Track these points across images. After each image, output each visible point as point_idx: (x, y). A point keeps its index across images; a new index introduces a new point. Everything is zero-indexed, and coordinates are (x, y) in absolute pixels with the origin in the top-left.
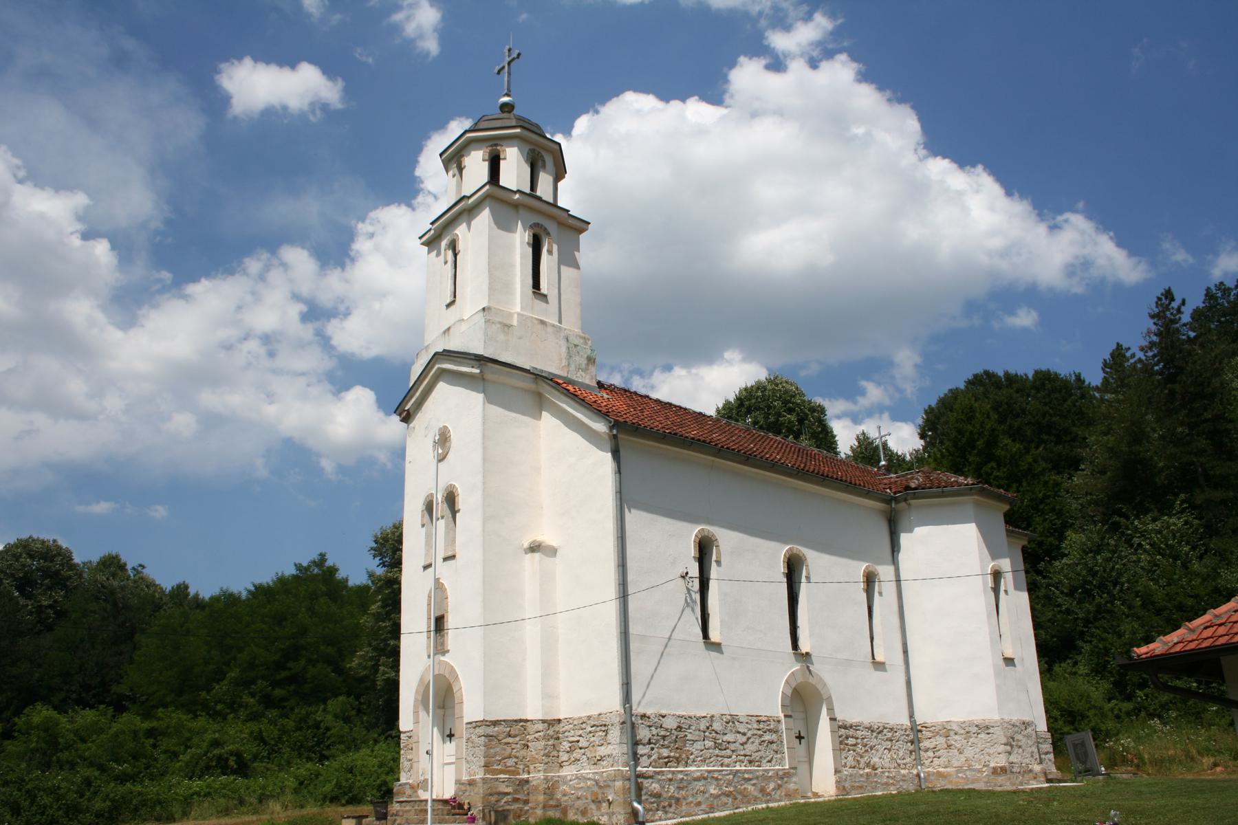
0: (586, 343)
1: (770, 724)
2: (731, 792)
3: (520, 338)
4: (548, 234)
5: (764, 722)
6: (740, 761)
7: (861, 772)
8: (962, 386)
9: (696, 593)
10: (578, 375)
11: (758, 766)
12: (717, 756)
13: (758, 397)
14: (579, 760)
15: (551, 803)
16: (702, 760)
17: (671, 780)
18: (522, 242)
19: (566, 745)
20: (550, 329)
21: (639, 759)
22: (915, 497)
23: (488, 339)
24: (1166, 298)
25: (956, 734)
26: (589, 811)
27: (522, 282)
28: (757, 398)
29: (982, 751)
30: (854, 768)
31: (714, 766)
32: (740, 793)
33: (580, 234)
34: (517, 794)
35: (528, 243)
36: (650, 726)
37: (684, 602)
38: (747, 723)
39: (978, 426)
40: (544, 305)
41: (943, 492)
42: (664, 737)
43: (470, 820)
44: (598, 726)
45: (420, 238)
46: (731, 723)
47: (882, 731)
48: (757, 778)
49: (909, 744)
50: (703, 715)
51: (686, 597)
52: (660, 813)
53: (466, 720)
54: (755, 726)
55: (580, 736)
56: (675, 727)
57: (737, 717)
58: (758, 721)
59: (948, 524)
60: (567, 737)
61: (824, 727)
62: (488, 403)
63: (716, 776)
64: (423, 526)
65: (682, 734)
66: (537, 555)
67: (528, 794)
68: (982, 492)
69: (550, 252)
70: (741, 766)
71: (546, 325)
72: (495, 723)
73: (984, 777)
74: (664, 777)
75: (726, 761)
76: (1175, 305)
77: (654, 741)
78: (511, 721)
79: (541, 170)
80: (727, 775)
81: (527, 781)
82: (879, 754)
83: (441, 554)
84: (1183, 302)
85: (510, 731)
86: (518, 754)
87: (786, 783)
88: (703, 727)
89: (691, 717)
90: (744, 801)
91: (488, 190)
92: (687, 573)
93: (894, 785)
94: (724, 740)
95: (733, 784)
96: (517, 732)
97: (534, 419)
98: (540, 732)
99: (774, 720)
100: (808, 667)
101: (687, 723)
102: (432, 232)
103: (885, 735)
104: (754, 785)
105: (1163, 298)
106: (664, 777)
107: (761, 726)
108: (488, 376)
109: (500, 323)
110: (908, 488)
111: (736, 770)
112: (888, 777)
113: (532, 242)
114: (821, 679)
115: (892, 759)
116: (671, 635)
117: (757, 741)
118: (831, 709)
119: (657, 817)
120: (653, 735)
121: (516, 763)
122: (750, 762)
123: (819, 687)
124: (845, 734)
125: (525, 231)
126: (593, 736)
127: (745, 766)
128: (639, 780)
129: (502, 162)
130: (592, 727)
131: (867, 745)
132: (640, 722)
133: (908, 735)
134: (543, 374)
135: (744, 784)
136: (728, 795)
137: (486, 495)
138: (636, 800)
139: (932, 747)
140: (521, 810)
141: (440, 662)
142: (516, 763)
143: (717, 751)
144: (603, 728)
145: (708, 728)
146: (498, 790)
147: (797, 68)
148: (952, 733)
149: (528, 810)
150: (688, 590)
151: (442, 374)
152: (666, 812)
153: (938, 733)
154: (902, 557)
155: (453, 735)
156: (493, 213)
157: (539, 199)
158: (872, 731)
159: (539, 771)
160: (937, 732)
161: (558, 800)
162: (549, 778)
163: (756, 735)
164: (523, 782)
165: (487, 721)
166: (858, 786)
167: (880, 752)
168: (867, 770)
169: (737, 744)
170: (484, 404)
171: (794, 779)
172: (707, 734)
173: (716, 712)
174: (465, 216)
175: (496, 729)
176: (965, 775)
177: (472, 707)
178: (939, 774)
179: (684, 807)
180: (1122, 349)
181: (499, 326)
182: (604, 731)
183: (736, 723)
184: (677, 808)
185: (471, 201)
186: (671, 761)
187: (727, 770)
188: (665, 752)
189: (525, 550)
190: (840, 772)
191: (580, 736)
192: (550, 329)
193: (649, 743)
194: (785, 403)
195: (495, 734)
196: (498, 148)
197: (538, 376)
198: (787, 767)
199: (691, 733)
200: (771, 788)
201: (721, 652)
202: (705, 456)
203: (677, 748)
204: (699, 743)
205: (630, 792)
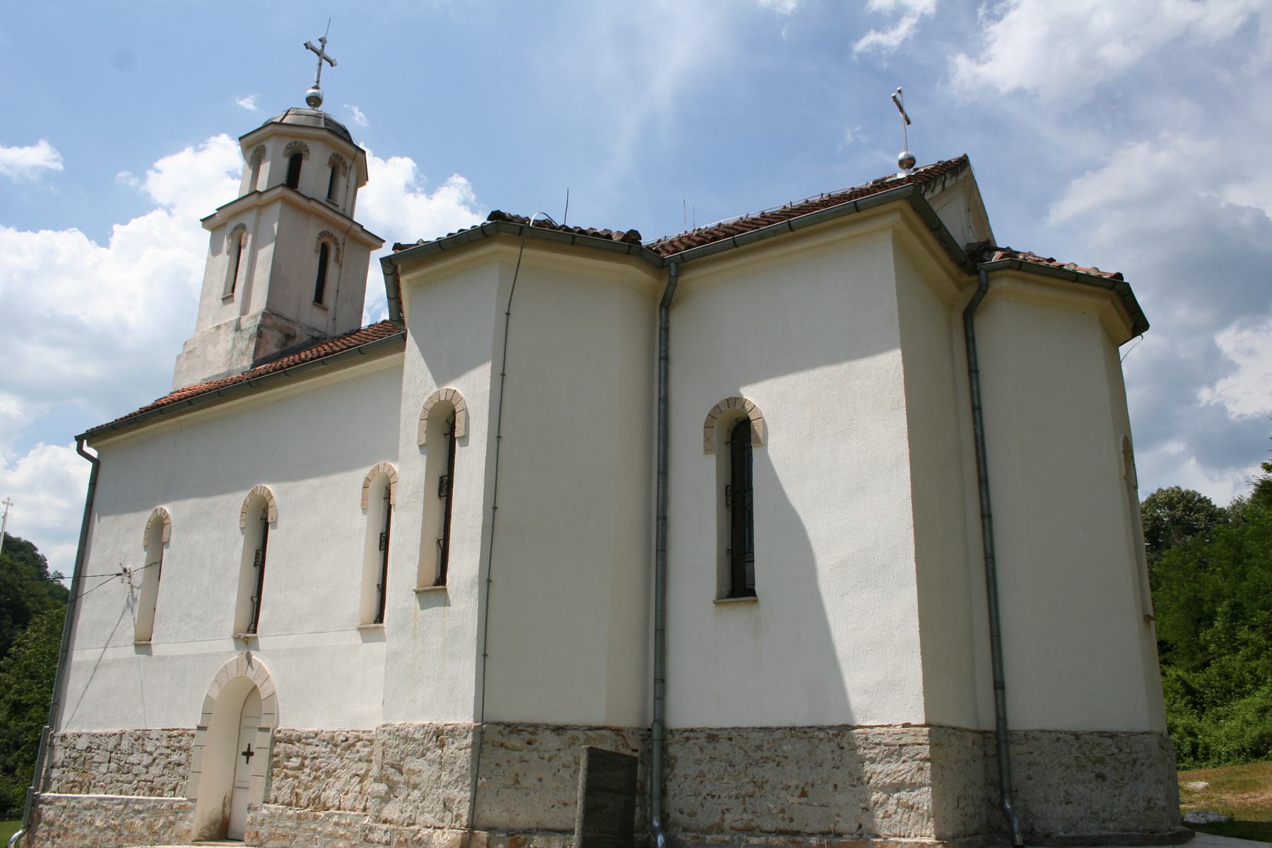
1: (181, 740)
5: (175, 737)
8: (1125, 281)
11: (158, 796)
31: (112, 794)
37: (125, 602)
38: (157, 739)
42: (75, 759)
51: (129, 596)
58: (169, 737)
63: (104, 805)
75: (126, 786)
88: (110, 747)
103: (358, 752)
104: (143, 819)
112: (337, 824)
131: (320, 768)
135: (133, 817)
145: (116, 747)
155: (252, 754)
158: (336, 745)
171: (190, 816)
172: (113, 754)
187: (118, 799)
199: (98, 754)
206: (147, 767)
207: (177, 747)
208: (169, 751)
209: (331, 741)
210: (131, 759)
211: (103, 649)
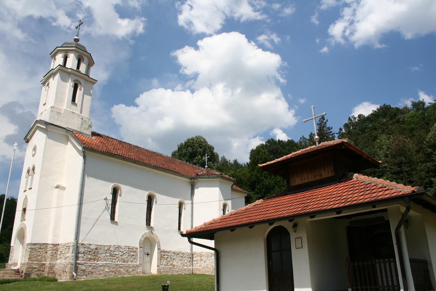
0: (89, 120)
1: (133, 249)
2: (114, 271)
3: (64, 117)
4: (81, 84)
5: (131, 248)
6: (119, 261)
7: (168, 267)
9: (110, 205)
10: (85, 131)
11: (126, 263)
12: (110, 259)
13: (191, 142)
14: (62, 258)
15: (51, 271)
16: (104, 260)
17: (90, 266)
18: (70, 85)
19: (59, 253)
20: (76, 115)
21: (79, 258)
23: (51, 117)
24: (322, 119)
25: (204, 256)
27: (68, 99)
28: (190, 143)
29: (212, 262)
30: (166, 265)
31: (109, 262)
32: (118, 271)
33: (94, 84)
34: (40, 268)
35: (72, 86)
36: (84, 248)
38: (124, 248)
39: (260, 156)
40: (75, 107)
41: (209, 177)
42: (90, 252)
43: (21, 276)
44: (67, 247)
46: (117, 248)
47: (179, 254)
48: (125, 267)
49: (189, 259)
50: (107, 245)
51: (106, 206)
52: (84, 276)
54: (127, 250)
55: (63, 250)
56: (95, 248)
57: (120, 246)
58: (128, 248)
60: (60, 250)
61: (156, 251)
62: (48, 138)
64: (26, 177)
65: (97, 251)
66: (58, 189)
67: (44, 268)
68: (222, 177)
69: (80, 90)
70: (119, 263)
71: (75, 114)
72: (35, 244)
73: (211, 270)
74: (87, 265)
75: (114, 260)
76: (324, 121)
77: (85, 253)
78: (41, 244)
79: (82, 62)
80: (113, 265)
81: (45, 264)
82: (177, 261)
83: (28, 187)
84: (327, 121)
85: (41, 247)
86: (42, 255)
87: (137, 269)
88: (106, 249)
89: (102, 246)
90: (119, 274)
91: (59, 67)
92: (106, 198)
93: (181, 272)
94: (114, 254)
95: (115, 268)
96: (43, 248)
97: (65, 144)
99: (135, 248)
100: (152, 232)
101: (100, 247)
102: (44, 80)
103: (180, 255)
104: (124, 269)
105: (321, 119)
106: (87, 265)
107: (130, 250)
108: (49, 129)
109: (56, 112)
110: (197, 175)
111: (117, 264)
112: (179, 269)
113: (74, 86)
114: (156, 236)
115: (182, 263)
116: (98, 218)
117: (127, 255)
118: (159, 246)
119: (83, 278)
120: (85, 251)
121: (41, 258)
122: (124, 261)
123: (155, 238)
124: (163, 255)
125: (72, 82)
126: (66, 250)
127: (121, 263)
128: (77, 265)
129: (68, 58)
130: (66, 247)
132: (81, 246)
133: (189, 256)
134: (71, 130)
136: (113, 272)
137: (42, 169)
138: (74, 272)
139: (196, 260)
140: (41, 274)
141: (23, 223)
142: (41, 258)
143: (111, 257)
144: (69, 247)
146: (32, 267)
148: (203, 256)
149: (44, 274)
150: (107, 204)
152: (87, 276)
154: (195, 197)
156: (60, 74)
157: (80, 72)
158: (175, 254)
159: (49, 261)
160: (198, 255)
161: (54, 271)
162: (51, 263)
163: (127, 253)
164: (43, 264)
165: (32, 243)
166: (166, 271)
167: (177, 261)
168: (171, 266)
169: (119, 255)
170: (46, 138)
172: (107, 251)
173: (112, 244)
174: (53, 76)
175: (35, 246)
176: (205, 269)
177: (28, 240)
178: (197, 269)
179: (94, 275)
180: (312, 134)
181: (56, 113)
183: (120, 248)
184: (91, 275)
185: (55, 70)
186: (92, 260)
187: (113, 264)
188: (89, 256)
189: (55, 187)
190: (159, 266)
192: (76, 115)
193: (84, 253)
194: (200, 145)
195: (34, 248)
196: (67, 53)
197: (67, 130)
198: (138, 264)
199: (101, 251)
200: (130, 270)
201: (117, 225)
202: (119, 160)
203: (95, 255)
204: (104, 254)
205: (73, 269)
206: (121, 255)
208: (129, 252)
210: (115, 253)
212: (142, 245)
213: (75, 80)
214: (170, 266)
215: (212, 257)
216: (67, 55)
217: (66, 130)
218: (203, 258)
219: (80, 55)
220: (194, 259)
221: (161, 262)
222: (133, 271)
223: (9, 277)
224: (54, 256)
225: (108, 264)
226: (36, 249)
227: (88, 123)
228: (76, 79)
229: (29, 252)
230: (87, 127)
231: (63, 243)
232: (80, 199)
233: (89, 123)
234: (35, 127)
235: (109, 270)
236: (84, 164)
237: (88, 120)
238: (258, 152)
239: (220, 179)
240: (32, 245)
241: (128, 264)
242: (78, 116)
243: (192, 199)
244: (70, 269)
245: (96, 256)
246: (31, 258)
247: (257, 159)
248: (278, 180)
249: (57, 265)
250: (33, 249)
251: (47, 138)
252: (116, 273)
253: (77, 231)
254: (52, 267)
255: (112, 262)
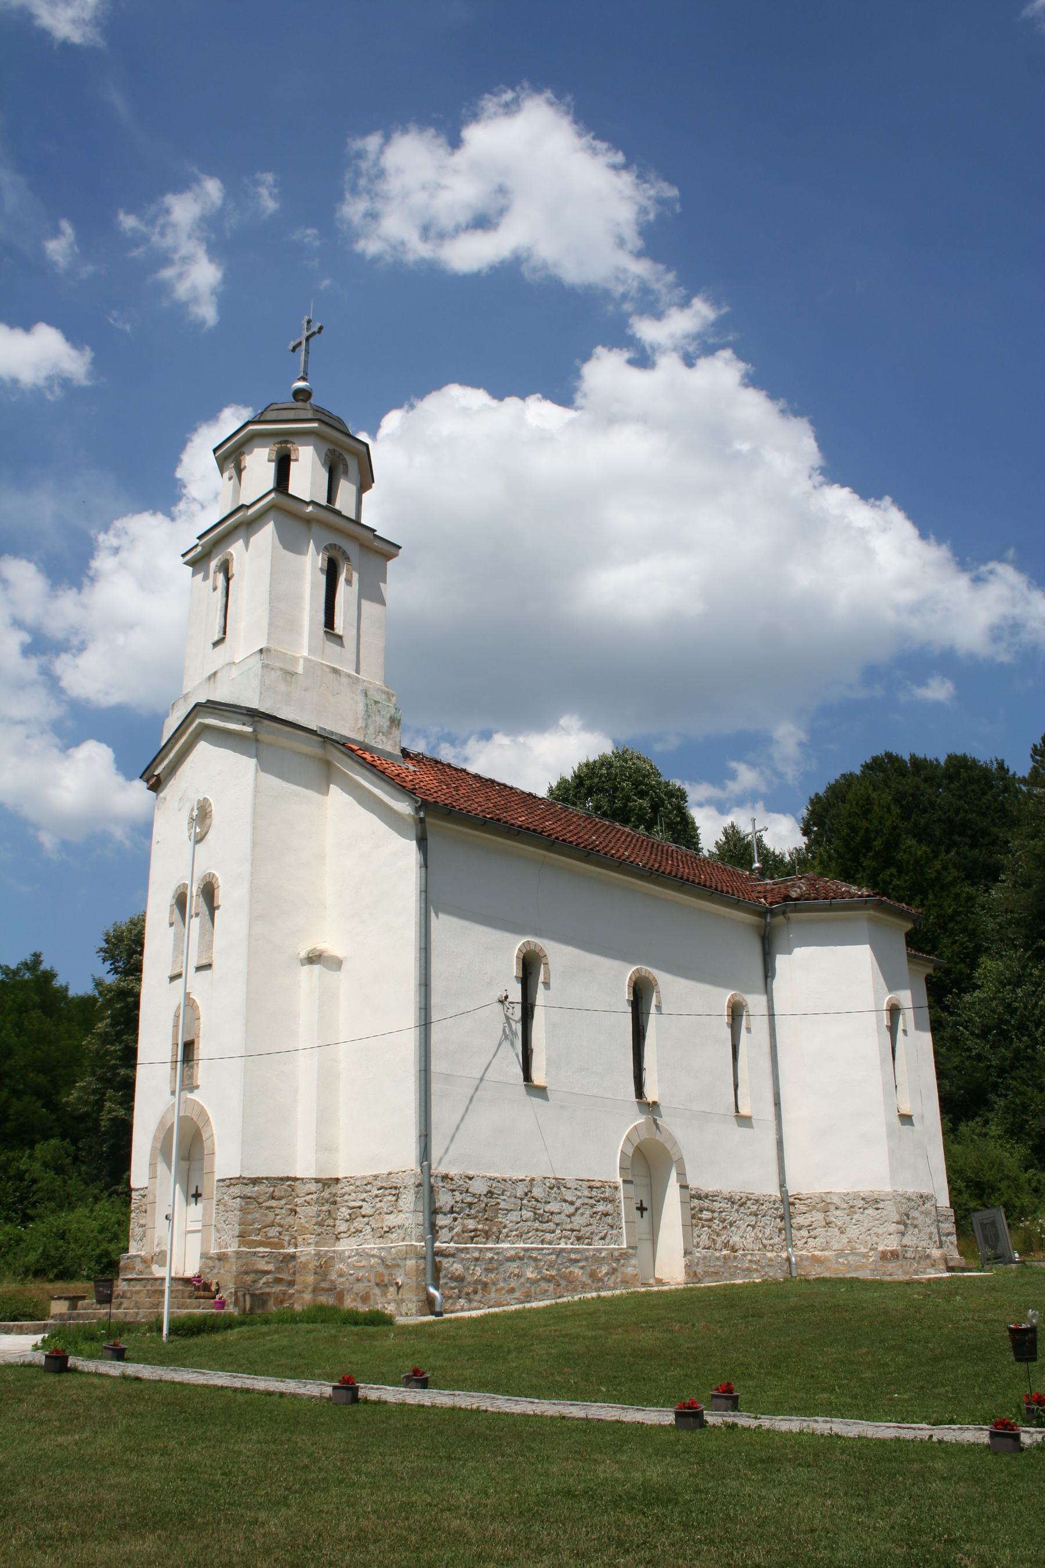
1: (605, 1192)
3: (306, 690)
4: (348, 559)
5: (597, 1188)
6: (565, 1237)
7: (717, 1254)
9: (516, 1022)
10: (378, 739)
12: (537, 1230)
13: (602, 775)
14: (361, 1231)
15: (324, 1285)
16: (517, 1236)
17: (477, 1259)
19: (345, 1212)
20: (344, 680)
21: (437, 1232)
22: (797, 909)
23: (265, 689)
25: (837, 1208)
26: (372, 1297)
31: (532, 1243)
34: (279, 1273)
35: (321, 569)
36: (453, 1191)
37: (502, 1033)
38: (576, 1189)
41: (831, 904)
42: (470, 1205)
43: (219, 1305)
44: (386, 1189)
45: (183, 555)
46: (555, 1189)
48: (587, 1259)
49: (778, 1220)
51: (505, 1027)
52: (462, 1301)
53: (217, 1177)
54: (586, 1193)
55: (364, 1200)
58: (589, 1187)
59: (835, 945)
61: (673, 1196)
62: (264, 770)
64: (171, 924)
65: (493, 1202)
66: (316, 968)
67: (294, 1273)
68: (880, 906)
69: (349, 582)
70: (566, 1244)
72: (255, 1181)
78: (275, 1179)
81: (293, 1257)
82: (740, 1232)
85: (274, 1191)
87: (623, 1266)
88: (520, 1193)
89: (505, 1180)
91: (273, 498)
92: (506, 997)
94: (547, 1210)
95: (556, 1267)
96: (283, 1194)
98: (312, 1194)
99: (610, 1187)
100: (655, 1121)
103: (749, 1208)
104: (582, 1268)
109: (281, 669)
112: (751, 1261)
113: (326, 568)
114: (670, 1134)
115: (757, 1238)
118: (681, 1175)
120: (456, 1202)
121: (280, 1233)
122: (579, 1239)
123: (668, 1146)
125: (318, 555)
126: (381, 1201)
127: (572, 1244)
128: (438, 1259)
129: (292, 464)
130: (378, 1189)
132: (441, 1184)
133: (777, 1209)
136: (549, 1280)
138: (432, 1285)
139: (807, 1224)
142: (280, 1233)
143: (537, 1224)
147: (669, 365)
148: (832, 1207)
150: (507, 1018)
151: (205, 731)
152: (470, 1301)
153: (814, 1207)
157: (338, 513)
158: (733, 1203)
159: (309, 1244)
161: (332, 1282)
162: (322, 1253)
163: (587, 1204)
164: (288, 1258)
165: (244, 1178)
167: (742, 1229)
168: (725, 1252)
170: (257, 771)
172: (525, 1201)
173: (537, 1174)
174: (242, 531)
175: (256, 1188)
178: (816, 1259)
179: (493, 1295)
181: (279, 673)
182: (394, 1195)
183: (563, 1189)
185: (251, 511)
187: (548, 1249)
188: (471, 1224)
189: (301, 960)
190: (691, 1253)
191: (364, 1200)
192: (344, 680)
193: (452, 1211)
194: (636, 784)
195: (254, 1195)
196: (289, 446)
197: (326, 739)
198: (625, 1246)
199: (504, 1200)
200: (604, 1272)
201: (546, 1099)
203: (487, 1219)
205: (425, 1275)
206: (569, 1216)
207: (601, 1198)
208: (592, 1201)
209: (731, 1200)
210: (548, 1207)
211: (478, 1081)
212: (629, 1172)
213: (330, 544)
214: (721, 1250)
215: (866, 1211)
216: (289, 450)
217: (321, 739)
218: (835, 1216)
219: (334, 450)
220: (799, 1220)
221: (695, 1235)
222: (613, 1273)
223: (178, 1308)
224: (326, 1224)
225: (533, 1249)
226: (261, 1201)
227: (388, 712)
228: (331, 542)
229: (238, 1213)
230: (386, 723)
231: (359, 1175)
232: (423, 1003)
233: (390, 709)
234: (192, 731)
235: (538, 1273)
236: (423, 869)
237: (384, 697)
238: (863, 806)
239: (876, 914)
240: (246, 1185)
241: (594, 1250)
242: (353, 683)
243: (769, 986)
244: (417, 1276)
245: (491, 1221)
246: (245, 1232)
247: (862, 832)
248: (950, 911)
249: (342, 1260)
250: (249, 1198)
251: (259, 771)
252: (559, 1285)
253: (423, 1128)
254: (323, 1267)
255: (542, 1242)
